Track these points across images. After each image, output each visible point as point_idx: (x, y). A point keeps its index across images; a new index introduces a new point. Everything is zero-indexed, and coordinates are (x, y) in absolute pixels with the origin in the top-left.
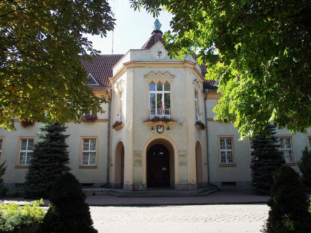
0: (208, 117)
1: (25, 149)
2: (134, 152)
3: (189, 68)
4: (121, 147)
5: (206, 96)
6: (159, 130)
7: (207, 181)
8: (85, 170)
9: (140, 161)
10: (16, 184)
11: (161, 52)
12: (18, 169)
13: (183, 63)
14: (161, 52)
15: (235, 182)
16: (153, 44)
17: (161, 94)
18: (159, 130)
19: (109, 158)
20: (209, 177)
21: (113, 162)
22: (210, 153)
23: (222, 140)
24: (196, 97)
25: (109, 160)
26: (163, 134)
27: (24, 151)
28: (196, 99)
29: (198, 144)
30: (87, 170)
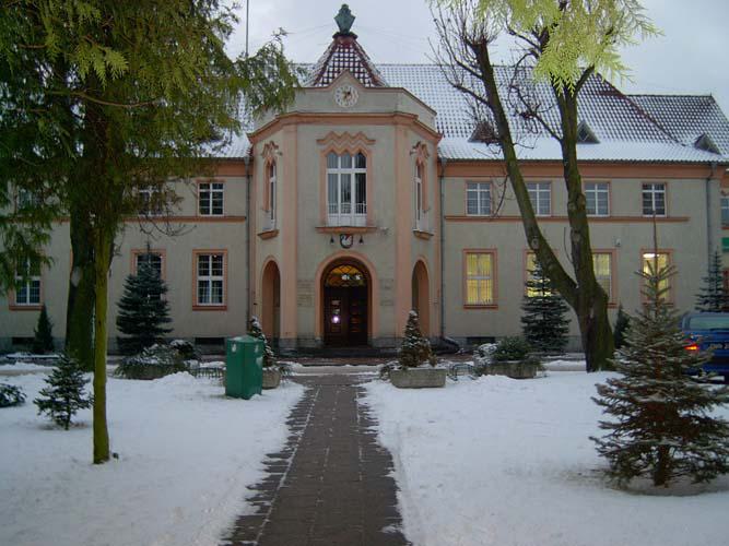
0: (446, 213)
1: (206, 273)
2: (299, 281)
3: (403, 124)
4: (272, 270)
5: (443, 171)
6: (344, 242)
7: (438, 335)
8: (202, 313)
9: (309, 297)
10: (14, 338)
11: (349, 93)
12: (469, 311)
13: (392, 117)
14: (349, 93)
15: (222, 339)
16: (617, 91)
17: (349, 176)
18: (344, 242)
19: (250, 292)
20: (442, 328)
21: (258, 299)
22: (445, 282)
23: (203, 258)
24: (419, 176)
25: (249, 296)
26: (352, 249)
27: (204, 278)
28: (418, 180)
29: (420, 268)
30: (209, 313)
